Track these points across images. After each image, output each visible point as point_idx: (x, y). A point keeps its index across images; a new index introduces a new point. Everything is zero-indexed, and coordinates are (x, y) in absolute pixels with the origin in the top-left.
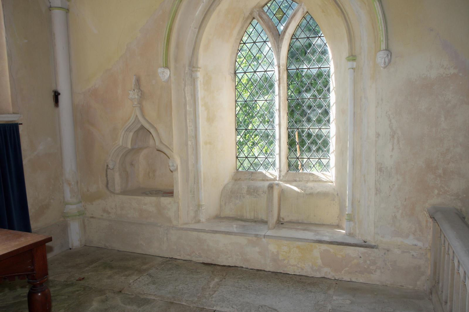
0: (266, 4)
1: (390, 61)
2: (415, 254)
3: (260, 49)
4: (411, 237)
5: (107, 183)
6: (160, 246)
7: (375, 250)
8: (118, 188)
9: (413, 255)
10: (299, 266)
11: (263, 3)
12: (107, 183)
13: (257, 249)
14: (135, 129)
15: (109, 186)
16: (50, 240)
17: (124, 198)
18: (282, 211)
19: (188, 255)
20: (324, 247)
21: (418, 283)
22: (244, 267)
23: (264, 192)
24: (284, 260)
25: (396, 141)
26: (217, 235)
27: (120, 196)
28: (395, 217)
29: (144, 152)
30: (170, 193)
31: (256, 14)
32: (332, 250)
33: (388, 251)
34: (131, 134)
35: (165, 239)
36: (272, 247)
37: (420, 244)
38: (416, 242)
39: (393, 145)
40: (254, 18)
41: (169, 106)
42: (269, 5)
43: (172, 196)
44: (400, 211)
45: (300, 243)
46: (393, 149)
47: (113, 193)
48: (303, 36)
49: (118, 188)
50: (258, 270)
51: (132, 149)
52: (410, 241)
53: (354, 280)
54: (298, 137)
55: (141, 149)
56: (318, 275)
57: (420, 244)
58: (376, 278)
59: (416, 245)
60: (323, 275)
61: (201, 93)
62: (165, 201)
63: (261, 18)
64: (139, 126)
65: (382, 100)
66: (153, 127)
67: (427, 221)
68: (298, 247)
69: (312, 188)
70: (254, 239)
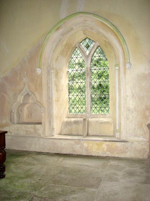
0: (82, 42)
1: (131, 67)
2: (143, 144)
3: (75, 98)
4: (141, 137)
5: (11, 119)
6: (34, 147)
7: (127, 143)
8: (16, 121)
9: (142, 144)
10: (97, 152)
11: (80, 41)
12: (11, 119)
13: (79, 146)
14: (24, 95)
15: (12, 120)
16: (6, 132)
17: (18, 125)
18: (89, 130)
19: (48, 150)
20: (107, 143)
21: (144, 155)
22: (73, 154)
23: (81, 123)
24: (90, 150)
25: (134, 98)
26: (62, 140)
27: (17, 125)
28: (135, 129)
29: (26, 106)
30: (40, 123)
31: (77, 46)
32: (110, 144)
33: (132, 143)
34: (23, 97)
35: (38, 143)
36: (85, 145)
37: (145, 140)
38: (143, 139)
39: (133, 100)
40: (76, 48)
41: (41, 85)
42: (83, 42)
43: (41, 124)
44: (137, 127)
45: (97, 142)
46: (133, 102)
47: (13, 123)
48: (97, 55)
49: (16, 121)
50: (79, 155)
51: (23, 104)
52: (141, 139)
53: (119, 156)
54: (119, 109)
55: (26, 104)
56: (105, 155)
57: (145, 140)
58: (128, 155)
59: (143, 140)
60: (107, 155)
61: (54, 79)
62: (38, 126)
63: (80, 47)
64: (26, 93)
65: (128, 82)
66: (33, 93)
67: (147, 130)
68: (96, 144)
69: (102, 120)
70: (78, 141)
